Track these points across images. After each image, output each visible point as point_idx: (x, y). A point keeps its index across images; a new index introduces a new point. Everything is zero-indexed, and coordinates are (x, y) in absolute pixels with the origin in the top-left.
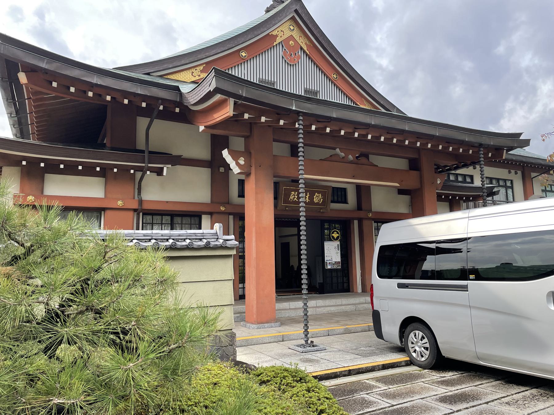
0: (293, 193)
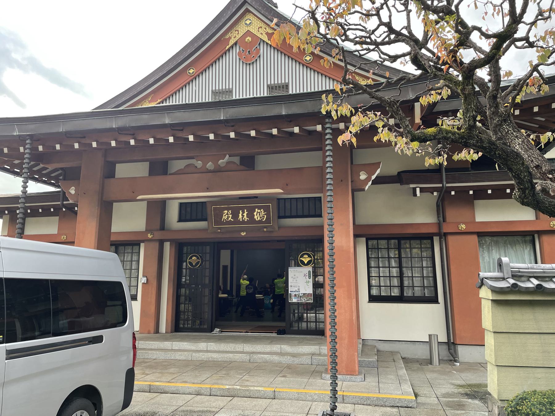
0: (226, 212)
